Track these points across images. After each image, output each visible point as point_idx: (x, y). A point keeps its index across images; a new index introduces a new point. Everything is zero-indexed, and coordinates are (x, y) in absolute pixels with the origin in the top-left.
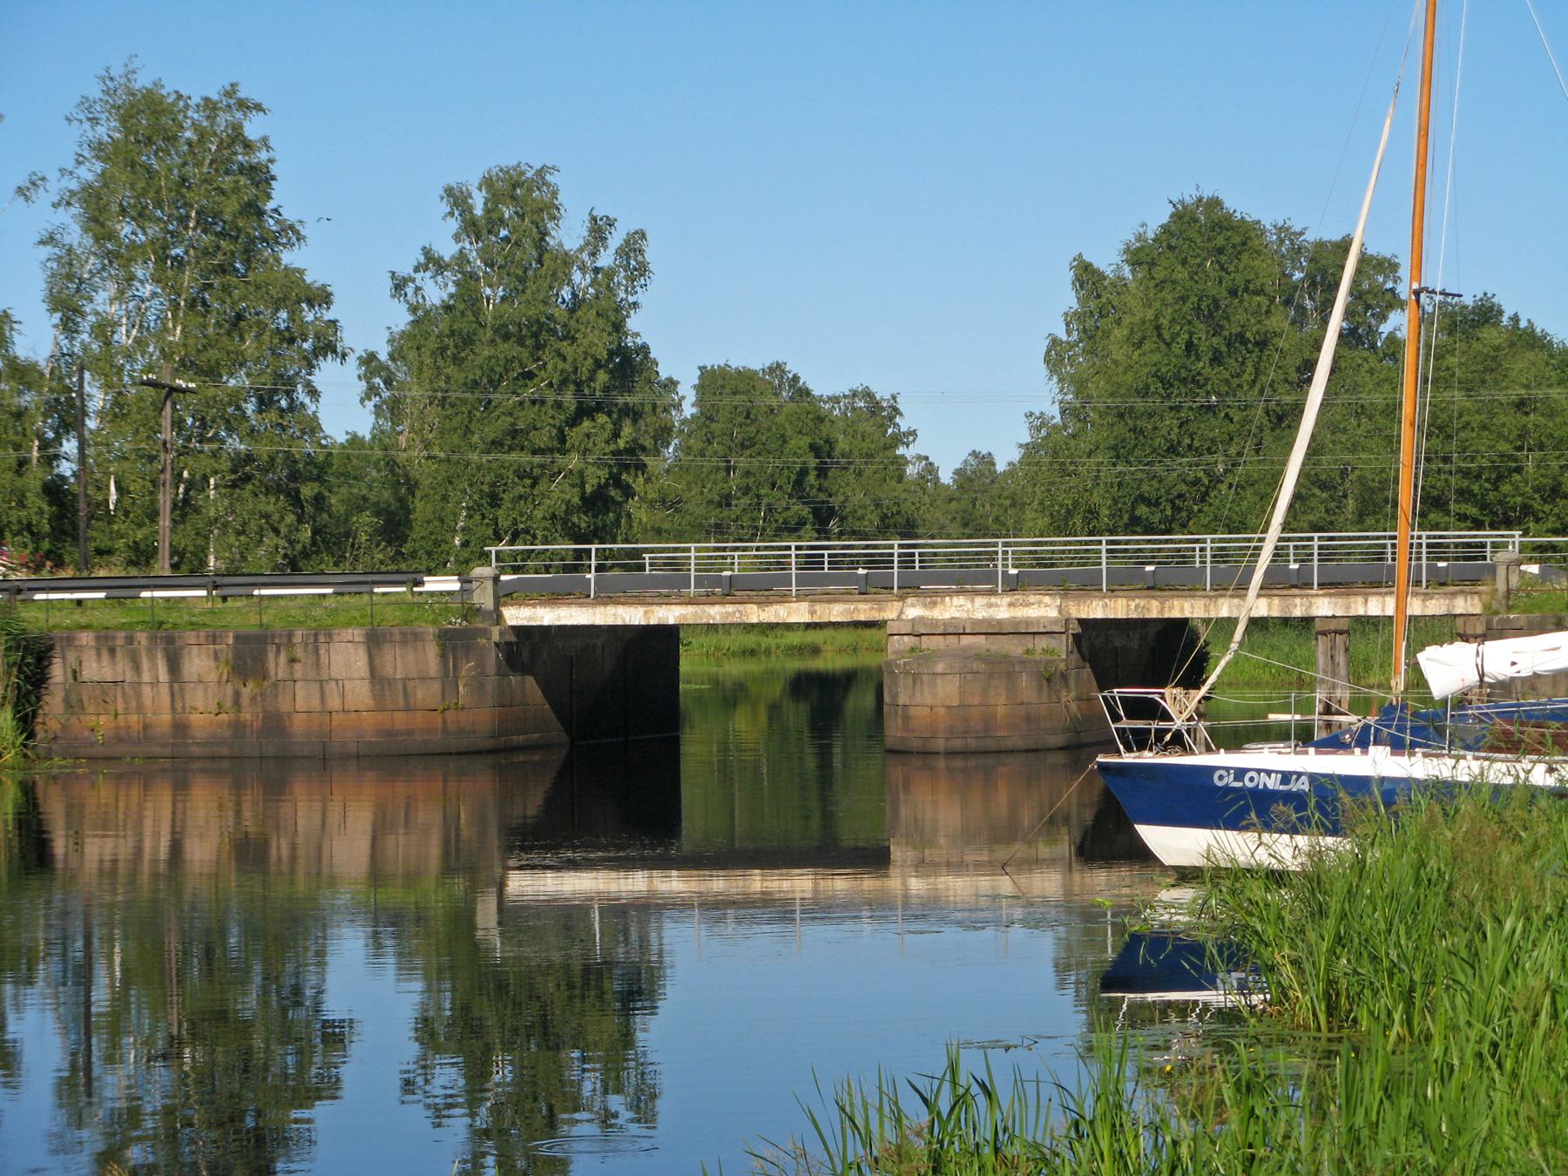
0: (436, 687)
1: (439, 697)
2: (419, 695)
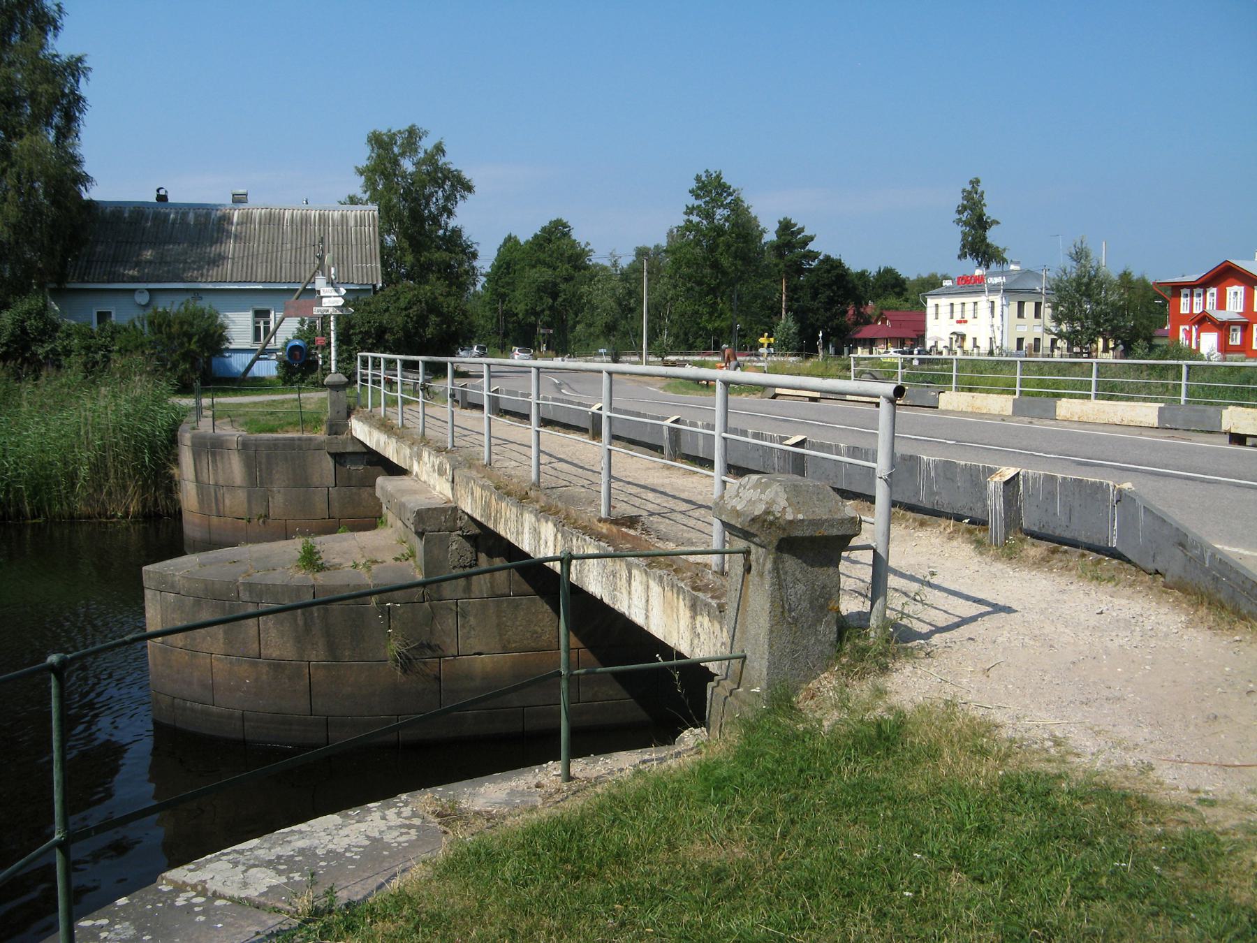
0: (242, 495)
1: (246, 505)
2: (227, 502)
